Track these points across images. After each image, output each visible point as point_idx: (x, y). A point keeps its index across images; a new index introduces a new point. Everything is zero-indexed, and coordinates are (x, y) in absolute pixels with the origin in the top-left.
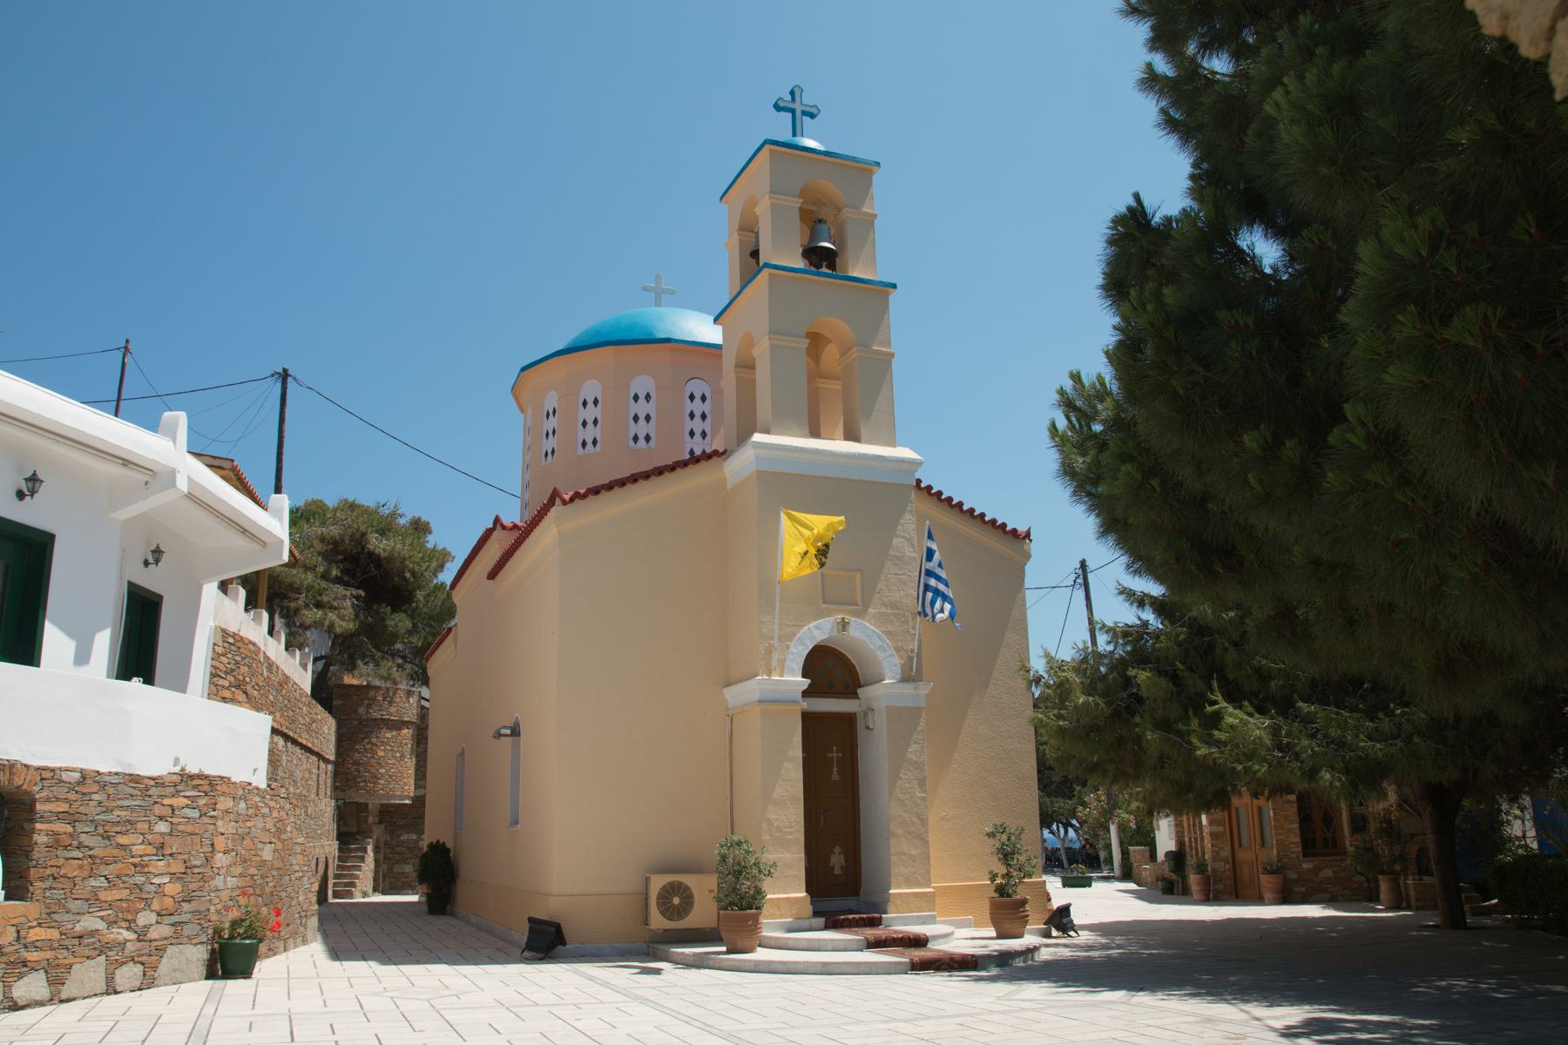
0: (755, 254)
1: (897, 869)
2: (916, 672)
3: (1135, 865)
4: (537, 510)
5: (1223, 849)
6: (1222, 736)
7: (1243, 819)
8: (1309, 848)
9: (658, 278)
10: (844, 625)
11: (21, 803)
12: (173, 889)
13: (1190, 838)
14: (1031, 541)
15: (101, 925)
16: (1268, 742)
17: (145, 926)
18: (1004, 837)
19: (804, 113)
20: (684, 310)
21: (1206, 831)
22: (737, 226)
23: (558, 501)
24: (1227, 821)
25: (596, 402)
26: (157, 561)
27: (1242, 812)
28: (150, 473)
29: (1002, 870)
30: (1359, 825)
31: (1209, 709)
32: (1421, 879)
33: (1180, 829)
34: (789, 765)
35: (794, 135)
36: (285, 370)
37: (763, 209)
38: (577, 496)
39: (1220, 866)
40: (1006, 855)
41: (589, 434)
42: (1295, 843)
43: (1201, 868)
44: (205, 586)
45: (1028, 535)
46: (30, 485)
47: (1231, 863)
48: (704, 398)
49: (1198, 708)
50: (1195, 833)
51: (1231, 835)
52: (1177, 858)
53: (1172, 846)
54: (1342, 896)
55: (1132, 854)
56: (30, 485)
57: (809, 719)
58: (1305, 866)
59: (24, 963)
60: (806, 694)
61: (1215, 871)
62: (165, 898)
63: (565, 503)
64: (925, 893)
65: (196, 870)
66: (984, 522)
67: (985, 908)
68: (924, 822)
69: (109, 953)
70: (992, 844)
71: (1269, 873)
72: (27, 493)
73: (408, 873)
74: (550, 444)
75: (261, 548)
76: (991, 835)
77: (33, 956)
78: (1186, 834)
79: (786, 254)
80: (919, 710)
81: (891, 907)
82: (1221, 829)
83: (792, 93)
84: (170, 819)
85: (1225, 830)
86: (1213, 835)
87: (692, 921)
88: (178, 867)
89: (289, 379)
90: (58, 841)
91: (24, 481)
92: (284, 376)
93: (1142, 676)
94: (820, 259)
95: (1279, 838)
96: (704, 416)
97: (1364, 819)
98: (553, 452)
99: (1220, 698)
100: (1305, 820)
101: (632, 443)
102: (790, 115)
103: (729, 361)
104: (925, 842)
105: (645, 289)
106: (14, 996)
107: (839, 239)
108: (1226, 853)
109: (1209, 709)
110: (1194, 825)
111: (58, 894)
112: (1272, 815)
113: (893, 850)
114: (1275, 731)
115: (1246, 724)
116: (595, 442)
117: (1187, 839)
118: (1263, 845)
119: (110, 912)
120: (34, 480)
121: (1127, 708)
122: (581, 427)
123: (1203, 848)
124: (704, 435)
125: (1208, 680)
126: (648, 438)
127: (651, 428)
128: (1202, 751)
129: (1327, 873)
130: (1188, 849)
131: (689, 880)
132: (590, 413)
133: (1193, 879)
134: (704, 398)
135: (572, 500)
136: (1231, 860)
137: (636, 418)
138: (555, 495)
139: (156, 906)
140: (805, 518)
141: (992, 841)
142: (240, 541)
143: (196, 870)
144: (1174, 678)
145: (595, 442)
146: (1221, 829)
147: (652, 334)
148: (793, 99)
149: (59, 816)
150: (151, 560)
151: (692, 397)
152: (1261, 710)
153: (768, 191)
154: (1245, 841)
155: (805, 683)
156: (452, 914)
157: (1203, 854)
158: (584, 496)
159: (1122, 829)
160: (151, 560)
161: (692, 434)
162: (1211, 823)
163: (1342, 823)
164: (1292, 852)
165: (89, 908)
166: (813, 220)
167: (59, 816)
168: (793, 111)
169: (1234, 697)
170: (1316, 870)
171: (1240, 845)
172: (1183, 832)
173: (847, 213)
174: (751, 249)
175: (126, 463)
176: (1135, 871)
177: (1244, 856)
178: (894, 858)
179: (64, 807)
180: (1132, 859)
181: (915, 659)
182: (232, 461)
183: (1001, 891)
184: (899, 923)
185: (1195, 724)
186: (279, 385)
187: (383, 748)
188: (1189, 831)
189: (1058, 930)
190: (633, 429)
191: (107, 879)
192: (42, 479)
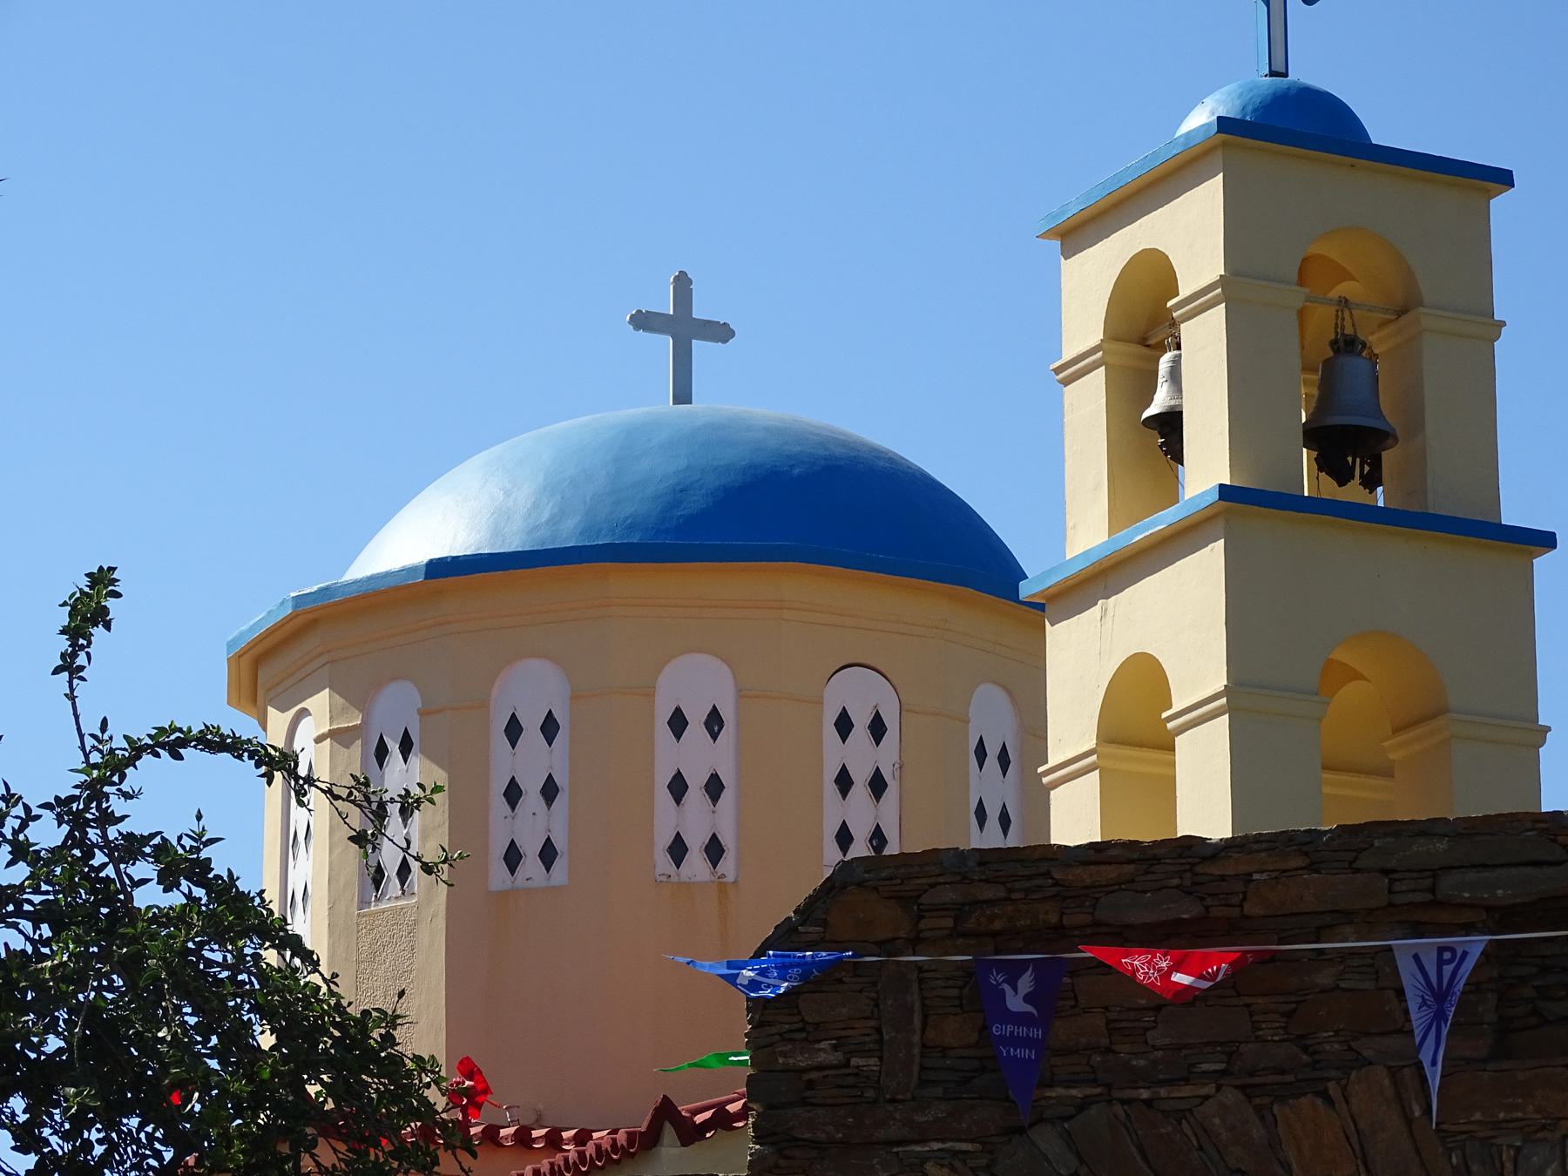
9: (683, 284)
20: (527, 549)
23: (669, 1133)
25: (550, 728)
44: (1384, 454)
48: (877, 729)
96: (878, 785)
101: (664, 862)
105: (643, 321)
116: (548, 854)
122: (727, 713)
126: (714, 850)
127: (725, 819)
134: (877, 729)
137: (513, 793)
138: (666, 1111)
140: (1434, 1063)
145: (548, 854)
151: (844, 725)
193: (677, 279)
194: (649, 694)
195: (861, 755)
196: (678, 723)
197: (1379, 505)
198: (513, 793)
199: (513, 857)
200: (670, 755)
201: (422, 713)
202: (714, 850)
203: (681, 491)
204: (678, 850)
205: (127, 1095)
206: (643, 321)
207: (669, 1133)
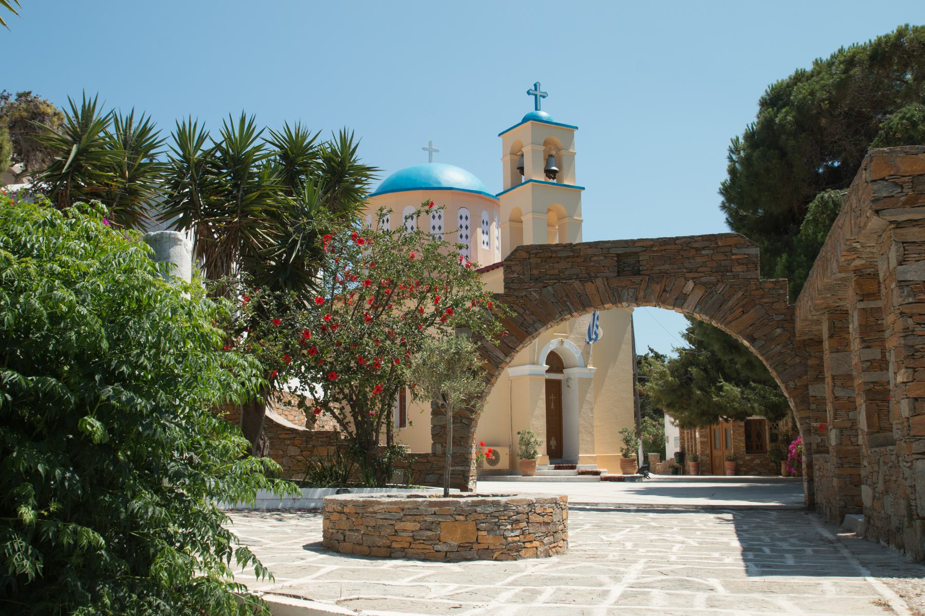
0: (521, 170)
1: (582, 446)
3: (651, 463)
6: (723, 394)
7: (717, 435)
8: (749, 449)
9: (430, 143)
10: (562, 342)
16: (739, 396)
18: (626, 434)
19: (541, 96)
21: (698, 440)
22: (509, 152)
27: (717, 432)
29: (626, 447)
30: (774, 438)
31: (718, 384)
34: (540, 401)
35: (536, 109)
37: (527, 150)
39: (704, 458)
40: (627, 441)
43: (695, 459)
48: (467, 218)
49: (714, 384)
51: (710, 442)
52: (681, 456)
53: (678, 450)
55: (650, 457)
57: (548, 382)
58: (747, 458)
60: (547, 371)
61: (702, 460)
64: (592, 457)
67: (618, 463)
68: (592, 426)
70: (622, 436)
71: (729, 460)
76: (621, 432)
79: (535, 172)
80: (591, 379)
81: (579, 462)
82: (706, 440)
83: (535, 85)
86: (702, 443)
87: (499, 466)
93: (693, 370)
94: (550, 173)
97: (776, 435)
99: (722, 380)
102: (534, 97)
104: (593, 435)
105: (424, 149)
107: (559, 166)
108: (708, 452)
109: (718, 384)
110: (691, 438)
113: (580, 438)
114: (742, 393)
115: (732, 390)
117: (686, 446)
118: (726, 448)
121: (686, 382)
123: (696, 450)
124: (467, 237)
125: (718, 371)
128: (715, 399)
129: (757, 461)
130: (687, 451)
131: (498, 449)
133: (690, 464)
134: (467, 218)
141: (621, 435)
144: (705, 370)
146: (706, 440)
147: (439, 183)
148: (536, 89)
151: (461, 217)
152: (737, 385)
153: (530, 142)
154: (718, 446)
155: (547, 367)
157: (696, 452)
159: (645, 443)
162: (701, 436)
166: (549, 158)
169: (728, 379)
170: (753, 460)
171: (715, 448)
173: (563, 152)
174: (517, 165)
176: (652, 466)
177: (716, 453)
178: (581, 442)
183: (625, 455)
184: (581, 466)
185: (713, 389)
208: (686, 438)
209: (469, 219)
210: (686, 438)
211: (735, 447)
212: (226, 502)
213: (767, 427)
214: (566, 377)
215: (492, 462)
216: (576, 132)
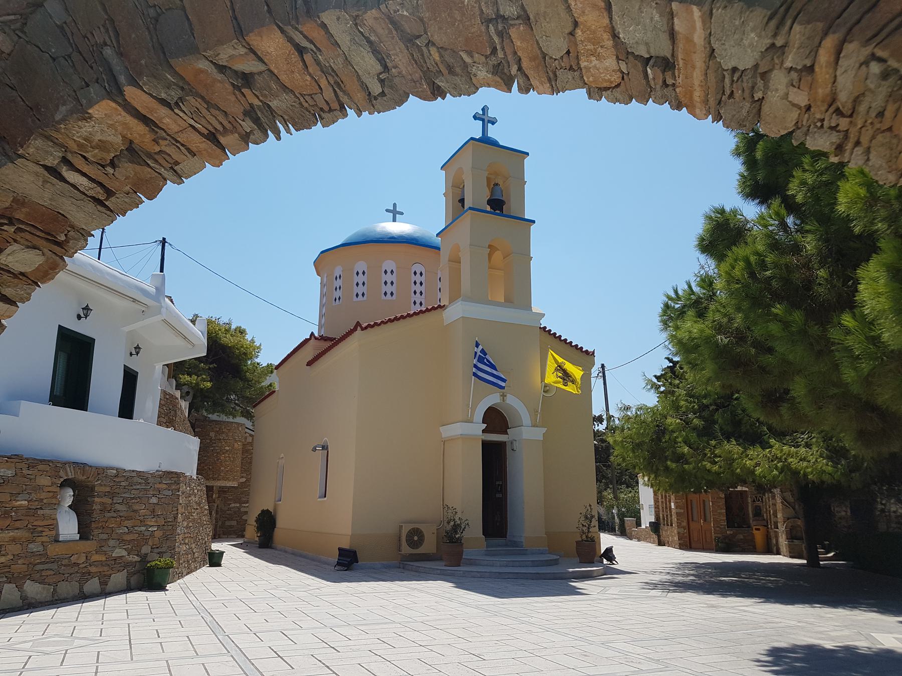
2: (470, 418)
4: (346, 332)
5: (683, 522)
9: (395, 205)
11: (86, 487)
12: (158, 534)
13: (663, 515)
14: (595, 356)
15: (124, 553)
17: (145, 554)
19: (489, 121)
21: (674, 512)
23: (359, 328)
24: (686, 507)
25: (364, 273)
26: (137, 353)
28: (146, 306)
32: (792, 542)
33: (658, 510)
36: (164, 239)
38: (370, 326)
41: (360, 290)
42: (723, 520)
45: (593, 352)
46: (85, 312)
47: (687, 529)
48: (421, 274)
50: (667, 512)
54: (747, 549)
56: (85, 312)
57: (486, 445)
59: (89, 573)
60: (484, 431)
62: (155, 538)
63: (363, 329)
65: (170, 524)
66: (561, 340)
69: (128, 569)
72: (83, 316)
73: (233, 526)
74: (338, 294)
75: (191, 347)
77: (93, 569)
78: (661, 513)
82: (682, 511)
83: (483, 109)
84: (158, 496)
85: (684, 511)
87: (421, 550)
88: (161, 521)
89: (166, 244)
90: (105, 508)
91: (82, 309)
92: (164, 242)
95: (714, 517)
98: (339, 298)
100: (729, 509)
103: (445, 255)
105: (387, 211)
106: (84, 591)
110: (666, 508)
111: (105, 536)
112: (711, 505)
116: (363, 294)
117: (661, 516)
119: (129, 546)
120: (87, 309)
130: (662, 521)
132: (361, 279)
134: (421, 274)
135: (366, 328)
136: (687, 527)
139: (150, 543)
142: (179, 342)
143: (170, 524)
145: (363, 294)
146: (682, 511)
149: (106, 494)
150: (134, 352)
151: (415, 273)
154: (695, 519)
156: (271, 547)
158: (379, 325)
160: (134, 352)
161: (415, 292)
162: (677, 507)
163: (748, 511)
164: (721, 525)
165: (119, 544)
167: (106, 494)
168: (483, 120)
172: (659, 511)
175: (134, 300)
179: (108, 489)
180: (626, 525)
181: (470, 410)
182: (171, 297)
186: (160, 247)
187: (223, 455)
188: (663, 511)
189: (608, 560)
190: (384, 288)
191: (127, 528)
192: (91, 308)
193: (394, 204)
194: (381, 267)
195: (418, 278)
196: (386, 272)
197: (487, 210)
198: (357, 284)
199: (357, 295)
200: (385, 278)
201: (342, 271)
202: (392, 294)
203: (390, 233)
204: (385, 294)
205: (692, 488)
206: (387, 211)
207: (359, 328)
208: (661, 508)
209: (424, 275)
210: (661, 508)
211: (715, 521)
212: (861, 457)
213: (749, 500)
214: (511, 439)
215: (412, 544)
216: (527, 161)
